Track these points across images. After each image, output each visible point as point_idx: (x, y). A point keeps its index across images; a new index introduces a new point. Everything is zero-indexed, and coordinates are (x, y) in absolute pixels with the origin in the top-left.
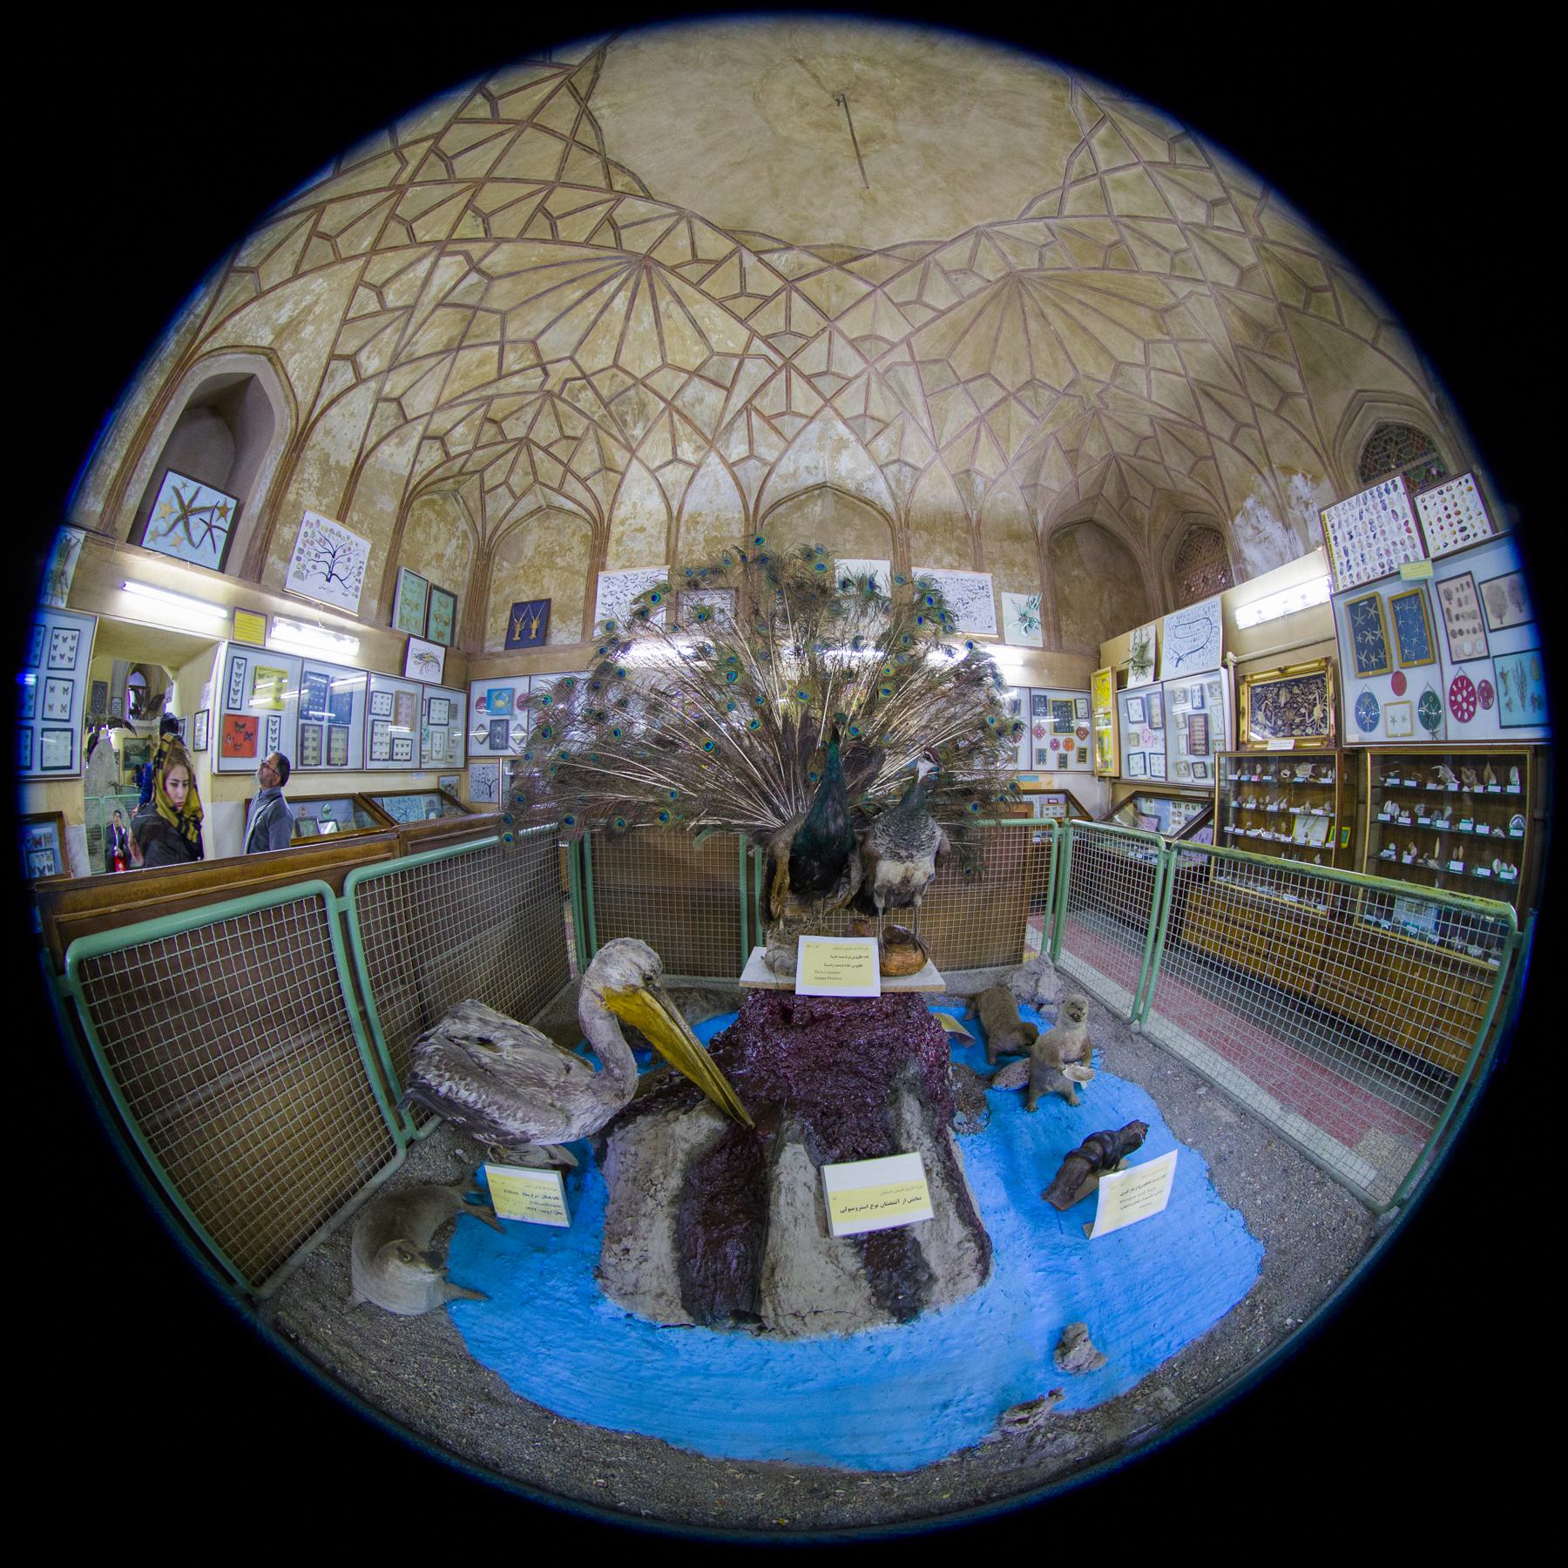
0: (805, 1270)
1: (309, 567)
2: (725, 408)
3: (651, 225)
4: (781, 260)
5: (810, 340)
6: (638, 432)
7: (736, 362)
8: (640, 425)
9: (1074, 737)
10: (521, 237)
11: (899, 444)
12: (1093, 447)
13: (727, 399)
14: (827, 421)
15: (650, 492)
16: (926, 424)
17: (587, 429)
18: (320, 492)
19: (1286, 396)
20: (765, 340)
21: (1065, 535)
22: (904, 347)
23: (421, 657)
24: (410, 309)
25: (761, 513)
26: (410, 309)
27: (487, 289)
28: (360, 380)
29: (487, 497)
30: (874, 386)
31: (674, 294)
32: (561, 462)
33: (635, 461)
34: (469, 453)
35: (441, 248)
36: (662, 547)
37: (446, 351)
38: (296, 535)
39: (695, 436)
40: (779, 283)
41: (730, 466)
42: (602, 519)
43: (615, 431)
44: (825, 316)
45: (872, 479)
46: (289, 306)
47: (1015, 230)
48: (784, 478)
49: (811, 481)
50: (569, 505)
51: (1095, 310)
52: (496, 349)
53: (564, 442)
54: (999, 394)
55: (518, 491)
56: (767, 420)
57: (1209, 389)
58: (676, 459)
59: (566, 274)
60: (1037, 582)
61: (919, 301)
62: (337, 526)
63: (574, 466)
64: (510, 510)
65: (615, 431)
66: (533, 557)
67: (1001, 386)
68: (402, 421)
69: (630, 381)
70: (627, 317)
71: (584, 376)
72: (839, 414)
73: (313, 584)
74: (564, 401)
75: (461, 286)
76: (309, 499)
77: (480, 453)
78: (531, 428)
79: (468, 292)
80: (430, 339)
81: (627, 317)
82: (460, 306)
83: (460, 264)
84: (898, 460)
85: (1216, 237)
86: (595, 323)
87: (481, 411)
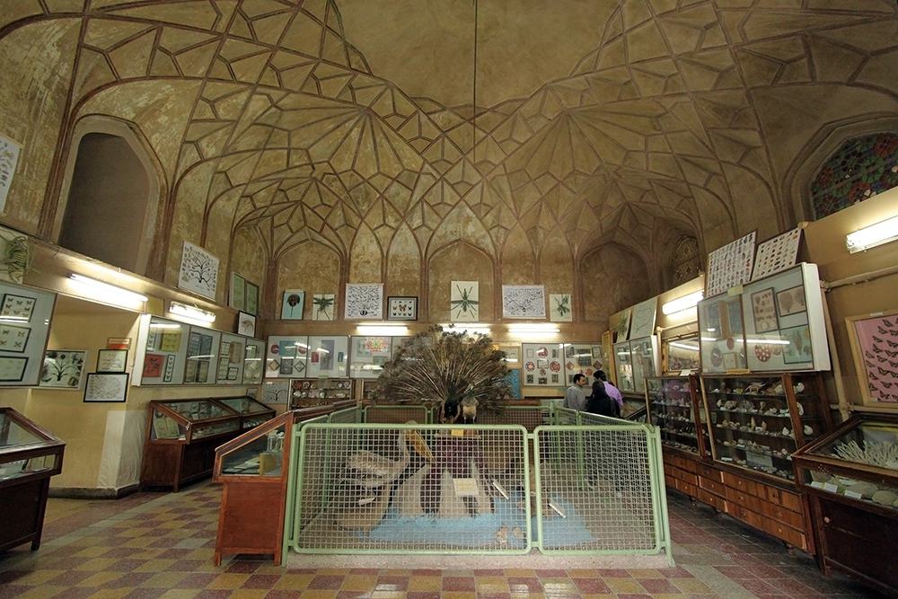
0: (446, 503)
1: (190, 274)
5: (454, 165)
7: (416, 176)
8: (366, 204)
10: (301, 92)
12: (613, 201)
14: (462, 208)
18: (189, 230)
19: (748, 149)
20: (431, 165)
21: (594, 253)
22: (502, 166)
23: (245, 323)
24: (235, 123)
25: (428, 257)
26: (235, 123)
27: (280, 117)
28: (203, 160)
30: (485, 189)
31: (385, 134)
35: (254, 88)
37: (256, 150)
39: (395, 214)
41: (413, 231)
42: (346, 255)
43: (352, 206)
44: (462, 152)
45: (484, 237)
46: (145, 96)
51: (614, 124)
52: (285, 152)
54: (553, 183)
55: (294, 229)
56: (432, 207)
57: (687, 158)
58: (385, 224)
59: (325, 114)
60: (571, 286)
61: (510, 138)
62: (201, 250)
63: (329, 221)
64: (288, 239)
65: (352, 206)
67: (555, 178)
68: (229, 187)
70: (359, 143)
73: (192, 285)
74: (324, 185)
75: (266, 114)
76: (184, 234)
77: (274, 207)
78: (304, 195)
79: (268, 117)
80: (246, 142)
81: (359, 143)
82: (265, 125)
83: (265, 100)
85: (703, 58)
86: (341, 144)
87: (276, 185)
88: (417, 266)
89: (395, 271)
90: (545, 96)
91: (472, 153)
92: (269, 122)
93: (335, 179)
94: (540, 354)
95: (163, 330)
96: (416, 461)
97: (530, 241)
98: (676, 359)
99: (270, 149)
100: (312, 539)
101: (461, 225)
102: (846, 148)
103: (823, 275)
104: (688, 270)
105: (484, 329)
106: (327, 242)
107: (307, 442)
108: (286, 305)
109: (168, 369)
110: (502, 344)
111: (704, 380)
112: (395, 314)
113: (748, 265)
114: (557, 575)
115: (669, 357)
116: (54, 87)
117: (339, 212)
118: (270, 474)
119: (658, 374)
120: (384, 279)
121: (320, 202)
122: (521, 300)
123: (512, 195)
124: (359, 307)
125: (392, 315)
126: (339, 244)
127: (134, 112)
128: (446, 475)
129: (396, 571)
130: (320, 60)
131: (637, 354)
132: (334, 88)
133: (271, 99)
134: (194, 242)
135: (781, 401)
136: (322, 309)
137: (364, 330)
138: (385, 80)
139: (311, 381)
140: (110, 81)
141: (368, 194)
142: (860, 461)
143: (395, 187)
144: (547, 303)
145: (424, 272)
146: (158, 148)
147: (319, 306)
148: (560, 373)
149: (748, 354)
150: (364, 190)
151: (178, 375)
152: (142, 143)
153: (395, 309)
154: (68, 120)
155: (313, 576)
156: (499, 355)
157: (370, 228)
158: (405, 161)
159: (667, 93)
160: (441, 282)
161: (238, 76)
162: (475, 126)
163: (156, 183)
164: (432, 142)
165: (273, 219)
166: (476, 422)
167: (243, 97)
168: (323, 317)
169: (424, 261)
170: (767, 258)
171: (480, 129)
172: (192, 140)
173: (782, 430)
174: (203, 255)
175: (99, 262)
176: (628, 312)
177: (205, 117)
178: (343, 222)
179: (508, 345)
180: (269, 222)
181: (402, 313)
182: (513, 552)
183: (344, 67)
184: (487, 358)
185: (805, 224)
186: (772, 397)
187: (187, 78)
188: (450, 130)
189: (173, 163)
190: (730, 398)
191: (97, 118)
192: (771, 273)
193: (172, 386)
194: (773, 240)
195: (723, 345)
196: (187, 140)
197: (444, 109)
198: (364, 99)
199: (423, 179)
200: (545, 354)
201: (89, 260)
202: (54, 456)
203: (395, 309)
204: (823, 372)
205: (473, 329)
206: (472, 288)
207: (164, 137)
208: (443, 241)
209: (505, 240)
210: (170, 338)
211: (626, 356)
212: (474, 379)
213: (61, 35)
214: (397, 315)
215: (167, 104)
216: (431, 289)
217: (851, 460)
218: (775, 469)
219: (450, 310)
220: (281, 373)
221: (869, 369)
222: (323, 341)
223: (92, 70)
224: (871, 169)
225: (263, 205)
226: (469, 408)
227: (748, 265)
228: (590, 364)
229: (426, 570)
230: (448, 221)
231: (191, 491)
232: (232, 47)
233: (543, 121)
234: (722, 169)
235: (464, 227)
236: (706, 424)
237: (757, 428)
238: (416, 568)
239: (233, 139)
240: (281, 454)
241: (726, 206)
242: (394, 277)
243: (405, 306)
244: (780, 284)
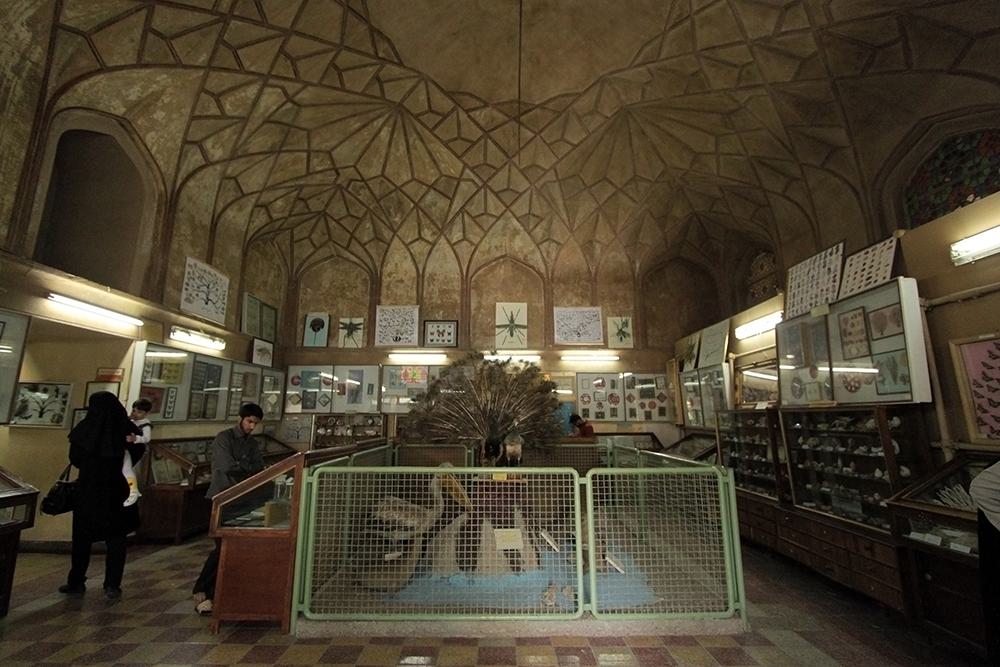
1: (194, 295)
2: (449, 210)
3: (402, 82)
4: (481, 116)
5: (498, 170)
6: (397, 219)
7: (456, 183)
9: (657, 401)
10: (320, 84)
11: (548, 230)
12: (679, 212)
13: (450, 206)
15: (406, 258)
16: (564, 217)
18: (193, 244)
19: (833, 150)
20: (472, 170)
22: (552, 171)
23: (260, 350)
24: (245, 120)
25: (470, 276)
26: (245, 120)
27: (297, 113)
28: (208, 163)
29: (296, 246)
30: (534, 196)
31: (418, 133)
34: (286, 218)
35: (265, 79)
38: (183, 274)
39: (432, 226)
40: (481, 133)
41: (452, 246)
42: (376, 271)
43: (384, 218)
44: (508, 157)
45: (533, 252)
47: (628, 74)
48: (483, 253)
52: (305, 155)
53: (349, 218)
54: (611, 190)
56: (473, 218)
57: (763, 161)
58: (420, 238)
59: (349, 110)
60: (632, 308)
61: (562, 139)
62: (207, 267)
63: (357, 235)
68: (240, 194)
72: (514, 216)
75: (280, 110)
76: (187, 249)
77: (293, 218)
78: (327, 206)
80: (258, 143)
88: (457, 285)
89: (432, 291)
90: (601, 90)
91: (517, 157)
92: (284, 120)
93: (363, 187)
94: (598, 385)
95: (162, 359)
96: (452, 509)
97: (584, 256)
98: (750, 389)
99: (288, 151)
100: (327, 603)
101: (507, 238)
102: (945, 146)
103: (923, 292)
104: (765, 289)
105: (534, 358)
106: (356, 260)
107: (320, 489)
108: (309, 330)
109: (169, 404)
110: (553, 374)
111: (783, 413)
112: (432, 341)
113: (834, 281)
114: (613, 643)
115: (743, 387)
116: (24, 75)
117: (368, 225)
118: (277, 527)
119: (730, 406)
120: (420, 300)
121: (346, 213)
122: (575, 324)
123: (564, 204)
126: (368, 260)
127: (125, 107)
128: (487, 525)
129: (424, 639)
130: (341, 47)
131: (706, 385)
132: (358, 81)
133: (285, 93)
134: (198, 258)
135: (872, 438)
136: (350, 334)
137: (397, 358)
138: (418, 72)
139: (340, 416)
140: (93, 69)
141: (400, 203)
142: (968, 509)
143: (431, 196)
144: (605, 327)
145: (465, 293)
146: (155, 148)
147: (346, 332)
148: (620, 407)
149: (835, 385)
150: (396, 198)
151: (180, 408)
152: (136, 144)
153: (432, 334)
154: (43, 112)
155: (326, 647)
156: (549, 386)
158: (443, 166)
159: (741, 85)
160: (484, 303)
161: (246, 64)
162: (521, 124)
163: (153, 189)
164: (474, 144)
165: (292, 232)
166: (522, 464)
167: (252, 91)
168: (350, 344)
169: (465, 279)
170: (856, 273)
171: (527, 128)
172: (196, 139)
173: (874, 471)
174: (210, 274)
175: (94, 284)
176: (695, 337)
177: (209, 114)
178: (372, 236)
179: (561, 374)
180: (288, 237)
181: (441, 338)
182: (561, 617)
183: (368, 55)
184: (535, 388)
185: (902, 233)
186: (863, 433)
187: (185, 67)
188: (493, 130)
189: (173, 166)
190: (814, 433)
191: (80, 113)
192: (861, 290)
193: (174, 423)
194: (863, 252)
195: (805, 373)
196: (189, 139)
197: (486, 105)
198: (394, 94)
199: (464, 186)
200: (602, 385)
201: (70, 278)
202: (24, 506)
203: (432, 334)
204: (923, 404)
205: (517, 356)
206: (520, 311)
207: (161, 135)
208: (487, 256)
209: (558, 254)
210: (171, 368)
211: (694, 387)
212: (519, 413)
213: (31, 12)
215: (163, 98)
216: (473, 312)
217: (956, 506)
218: (865, 516)
219: (494, 335)
220: (303, 408)
221: (978, 401)
222: (350, 371)
223: (72, 55)
224: (975, 171)
225: (280, 215)
226: (513, 448)
227: (834, 281)
228: (653, 396)
230: (493, 234)
231: (195, 544)
232: (237, 30)
233: (599, 120)
234: (803, 172)
235: (511, 241)
236: (786, 465)
237: (845, 469)
238: (448, 636)
239: (243, 139)
240: (290, 503)
241: (807, 216)
244: (873, 303)
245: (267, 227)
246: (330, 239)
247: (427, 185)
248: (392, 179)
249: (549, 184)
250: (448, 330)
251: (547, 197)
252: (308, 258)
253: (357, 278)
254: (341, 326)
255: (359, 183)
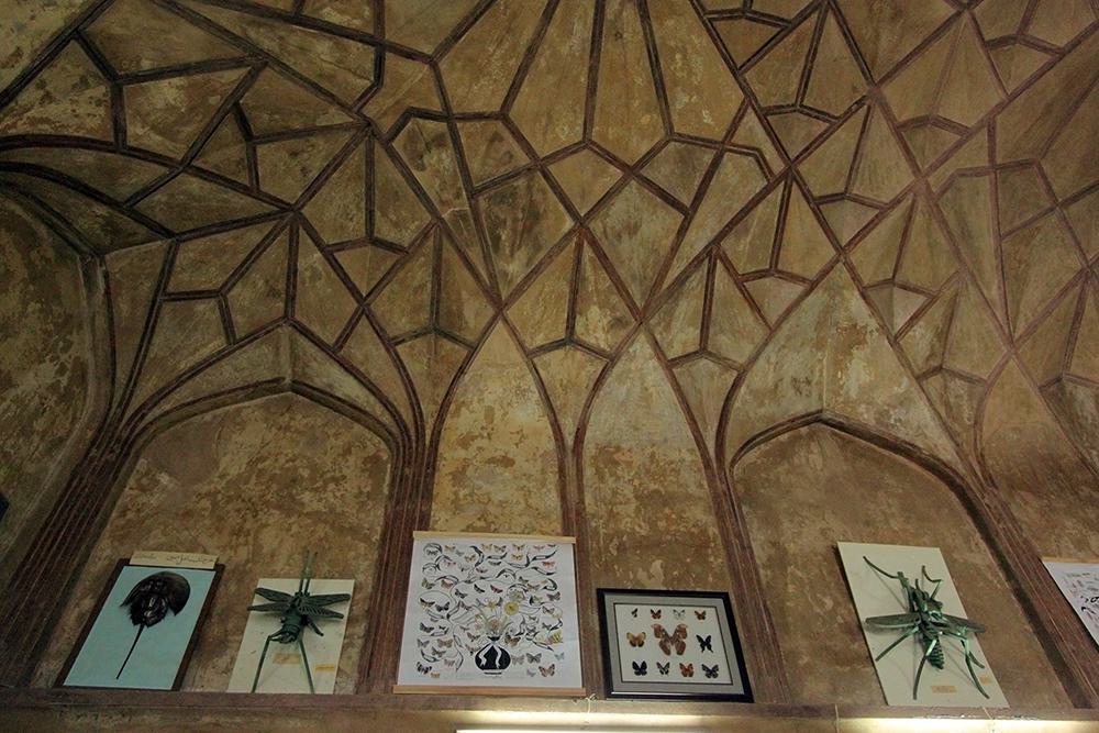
2: (675, 249)
5: (835, 122)
6: (515, 268)
7: (708, 157)
8: (522, 254)
13: (682, 231)
14: (834, 292)
16: (994, 293)
17: (425, 235)
20: (763, 115)
29: (167, 308)
32: (353, 290)
33: (500, 325)
36: (552, 500)
39: (615, 299)
41: (670, 365)
43: (475, 254)
45: (904, 401)
49: (800, 407)
50: (348, 388)
53: (368, 250)
56: (740, 281)
58: (570, 340)
63: (380, 306)
64: (207, 363)
66: (243, 479)
69: (523, 160)
71: (446, 116)
72: (855, 278)
74: (394, 157)
77: (194, 185)
78: (312, 190)
84: (939, 369)
88: (693, 481)
89: (614, 501)
108: (114, 615)
112: (640, 669)
120: (573, 521)
124: (468, 637)
125: (629, 674)
136: (290, 635)
141: (534, 216)
145: (727, 504)
153: (637, 642)
157: (521, 345)
158: (680, 100)
160: (792, 548)
168: (284, 679)
181: (675, 660)
203: (637, 642)
214: (653, 674)
225: (154, 142)
229: (31, 146)
230: (789, 338)
242: (612, 515)
243: (681, 631)
245: (86, 157)
246: (287, 316)
247: (623, 166)
248: (525, 132)
249: (963, 182)
250: (696, 628)
251: (952, 223)
252: (195, 371)
253: (347, 451)
254: (258, 601)
255: (430, 125)
